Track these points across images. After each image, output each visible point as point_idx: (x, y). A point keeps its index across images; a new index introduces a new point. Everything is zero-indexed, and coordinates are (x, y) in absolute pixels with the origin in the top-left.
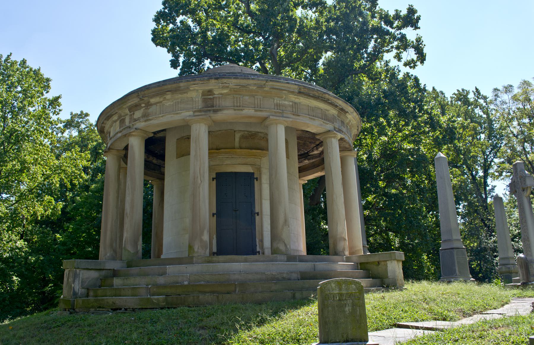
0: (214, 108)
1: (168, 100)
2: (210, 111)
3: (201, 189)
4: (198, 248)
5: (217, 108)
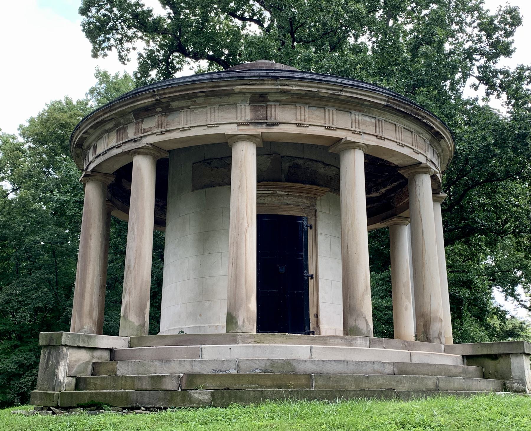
0: (269, 121)
1: (198, 104)
2: (261, 123)
3: (248, 235)
4: (244, 322)
5: (273, 120)
